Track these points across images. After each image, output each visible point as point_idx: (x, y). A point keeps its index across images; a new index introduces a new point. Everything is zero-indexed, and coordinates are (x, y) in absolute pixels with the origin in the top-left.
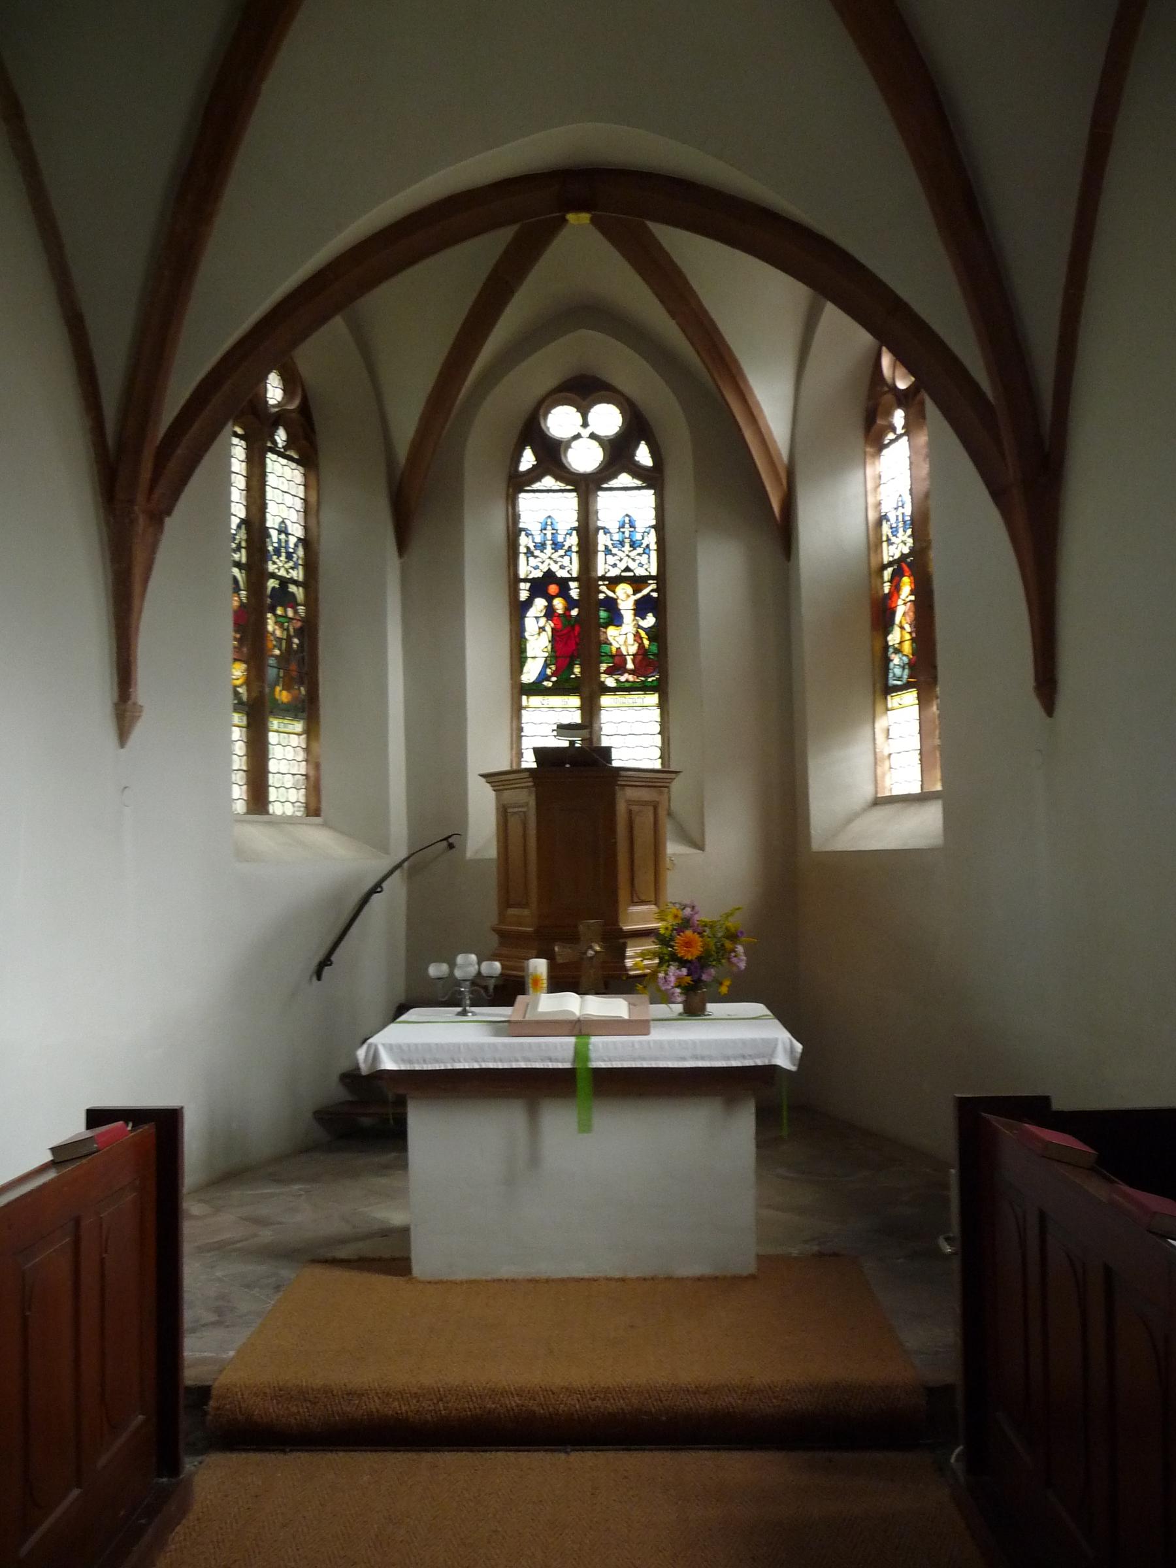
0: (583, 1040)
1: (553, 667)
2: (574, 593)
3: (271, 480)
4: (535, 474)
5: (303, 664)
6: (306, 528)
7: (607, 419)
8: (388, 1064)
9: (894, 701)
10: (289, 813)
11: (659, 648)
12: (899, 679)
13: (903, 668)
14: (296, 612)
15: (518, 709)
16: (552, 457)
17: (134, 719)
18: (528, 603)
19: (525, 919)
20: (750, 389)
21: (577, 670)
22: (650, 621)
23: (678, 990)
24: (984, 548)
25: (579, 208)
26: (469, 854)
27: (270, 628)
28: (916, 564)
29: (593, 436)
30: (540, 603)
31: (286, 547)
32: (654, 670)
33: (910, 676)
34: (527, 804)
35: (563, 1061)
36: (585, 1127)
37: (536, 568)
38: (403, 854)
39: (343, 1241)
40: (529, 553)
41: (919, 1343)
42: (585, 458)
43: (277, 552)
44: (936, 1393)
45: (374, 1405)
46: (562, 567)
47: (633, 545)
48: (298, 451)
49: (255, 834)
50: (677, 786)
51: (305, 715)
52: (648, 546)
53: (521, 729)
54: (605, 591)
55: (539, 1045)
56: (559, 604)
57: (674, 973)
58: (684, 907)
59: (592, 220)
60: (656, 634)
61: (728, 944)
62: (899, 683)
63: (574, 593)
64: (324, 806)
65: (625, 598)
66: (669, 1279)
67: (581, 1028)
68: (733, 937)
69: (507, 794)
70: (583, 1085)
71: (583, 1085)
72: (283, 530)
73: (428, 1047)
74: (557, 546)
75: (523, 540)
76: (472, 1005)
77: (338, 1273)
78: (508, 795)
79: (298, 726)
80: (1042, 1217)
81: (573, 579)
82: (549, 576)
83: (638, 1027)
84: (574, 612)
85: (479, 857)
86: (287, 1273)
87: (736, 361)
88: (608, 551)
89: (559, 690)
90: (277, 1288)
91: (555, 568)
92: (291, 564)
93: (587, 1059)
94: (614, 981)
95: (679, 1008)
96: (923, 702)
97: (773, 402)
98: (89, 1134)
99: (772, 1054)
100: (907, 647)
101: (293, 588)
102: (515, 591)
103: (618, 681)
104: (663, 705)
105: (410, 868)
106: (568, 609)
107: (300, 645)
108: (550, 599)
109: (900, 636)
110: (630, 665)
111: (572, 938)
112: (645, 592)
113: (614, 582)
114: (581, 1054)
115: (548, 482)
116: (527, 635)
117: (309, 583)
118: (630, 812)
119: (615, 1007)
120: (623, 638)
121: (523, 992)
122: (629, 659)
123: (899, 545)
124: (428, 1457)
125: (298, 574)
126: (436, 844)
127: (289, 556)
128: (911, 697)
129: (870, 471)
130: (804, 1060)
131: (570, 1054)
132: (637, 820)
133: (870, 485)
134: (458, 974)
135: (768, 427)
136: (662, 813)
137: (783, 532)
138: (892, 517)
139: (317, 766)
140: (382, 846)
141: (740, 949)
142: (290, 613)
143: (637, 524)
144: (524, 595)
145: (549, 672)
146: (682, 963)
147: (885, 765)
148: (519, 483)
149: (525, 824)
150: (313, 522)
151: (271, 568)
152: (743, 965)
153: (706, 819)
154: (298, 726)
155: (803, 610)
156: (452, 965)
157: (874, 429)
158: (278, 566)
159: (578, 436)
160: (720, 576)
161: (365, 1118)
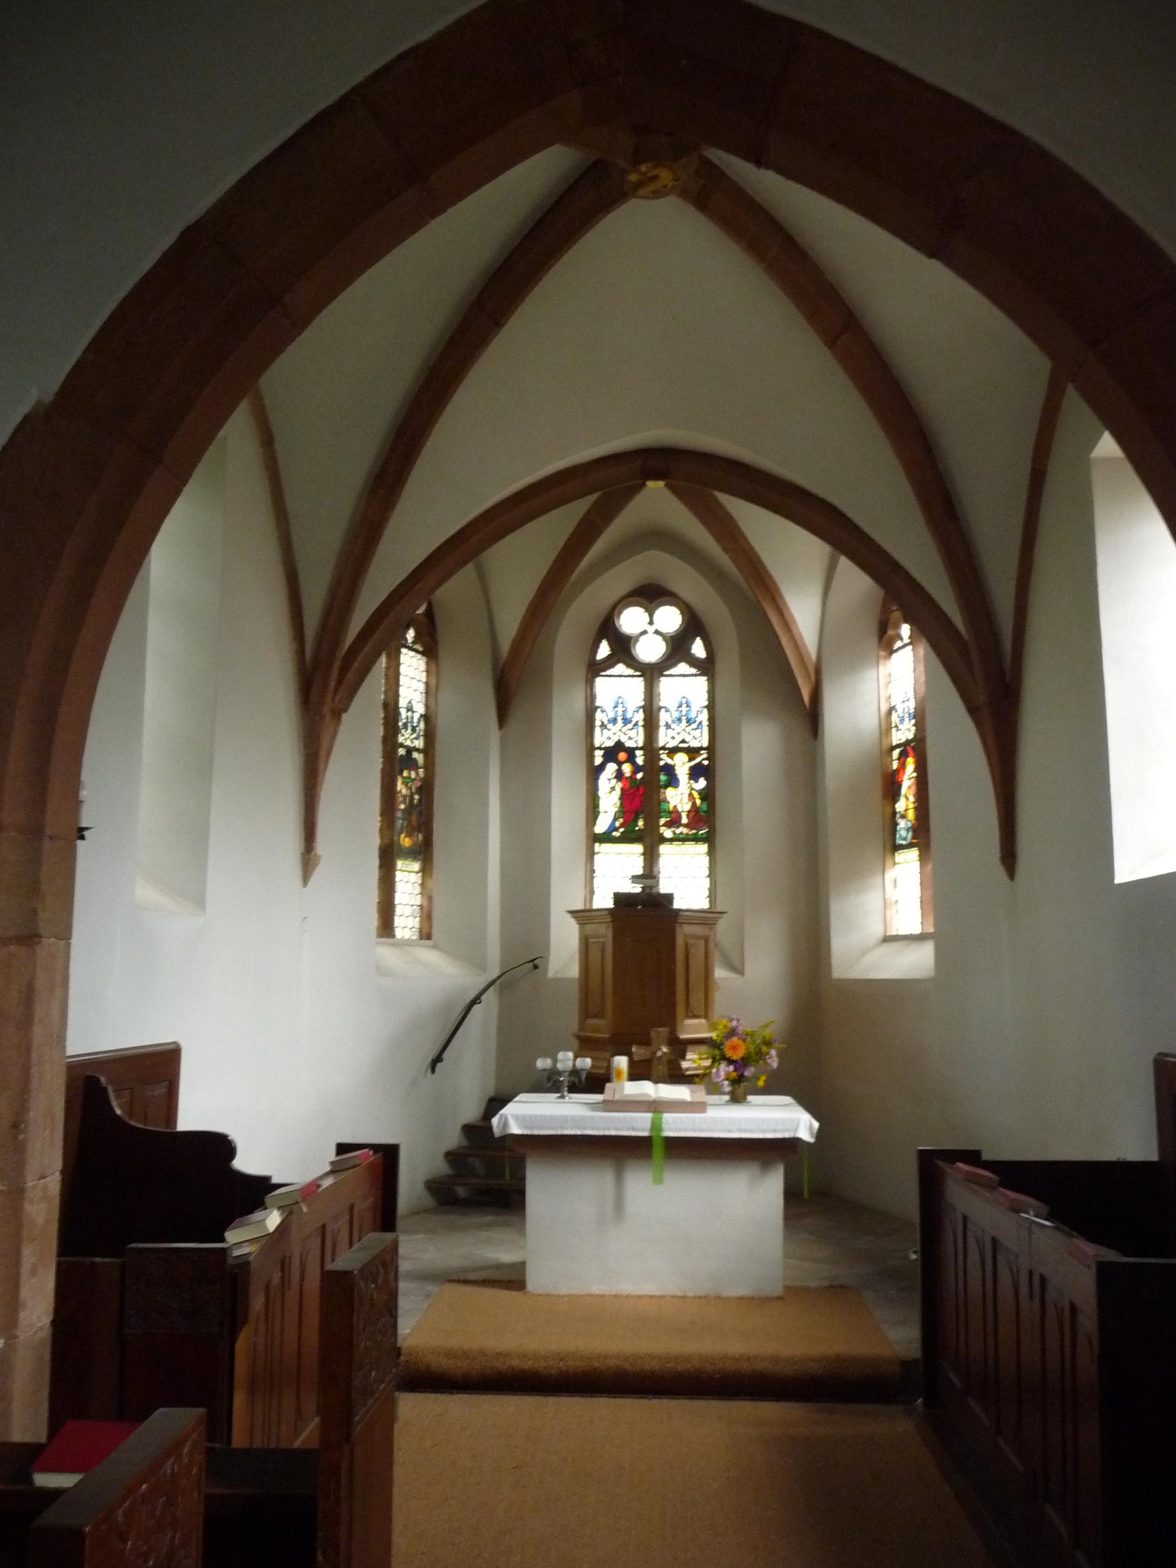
0: (658, 1115)
1: (621, 820)
2: (640, 760)
3: (403, 669)
4: (610, 662)
5: (422, 818)
6: (427, 706)
7: (670, 618)
8: (515, 1129)
9: (900, 856)
10: (407, 937)
11: (708, 805)
12: (905, 839)
13: (908, 830)
14: (417, 774)
15: (591, 854)
16: (623, 648)
17: (315, 865)
18: (602, 767)
19: (602, 1027)
20: (785, 604)
21: (641, 823)
22: (702, 783)
23: (726, 1083)
24: (962, 747)
25: (656, 477)
26: (550, 974)
27: (399, 788)
28: (917, 747)
29: (657, 632)
30: (611, 767)
31: (412, 722)
32: (705, 824)
33: (913, 838)
34: (605, 937)
35: (643, 1130)
36: (659, 1181)
37: (609, 738)
38: (497, 973)
39: (474, 1270)
40: (603, 726)
41: (898, 1336)
42: (650, 650)
43: (405, 726)
44: (906, 1365)
45: (515, 1362)
46: (630, 738)
47: (689, 721)
48: (423, 645)
49: (385, 953)
50: (722, 925)
51: (421, 857)
52: (700, 723)
53: (593, 871)
54: (665, 759)
55: (625, 1118)
56: (627, 769)
57: (724, 1069)
58: (731, 1020)
59: (667, 485)
61: (764, 1049)
62: (904, 843)
63: (640, 760)
64: (435, 932)
65: (682, 765)
66: (719, 1297)
67: (656, 1107)
68: (768, 1043)
69: (588, 927)
70: (658, 1149)
71: (658, 1149)
72: (410, 709)
73: (544, 1118)
74: (626, 721)
75: (599, 717)
76: (570, 1091)
77: (468, 1289)
78: (589, 928)
79: (416, 866)
80: (965, 1218)
81: (637, 748)
82: (619, 746)
83: (700, 1107)
84: (639, 776)
85: (559, 976)
86: (432, 1288)
87: (775, 584)
88: (668, 726)
89: (625, 839)
90: (428, 1296)
91: (624, 739)
92: (414, 735)
93: (661, 1130)
94: (677, 1077)
95: (727, 1098)
96: (923, 858)
97: (804, 612)
98: (339, 1158)
99: (796, 1130)
100: (911, 814)
101: (415, 755)
102: (591, 757)
103: (674, 833)
104: (711, 853)
105: (501, 984)
106: (634, 773)
107: (420, 800)
108: (620, 764)
109: (905, 804)
110: (685, 820)
111: (646, 1042)
112: (698, 760)
113: (673, 751)
114: (656, 1126)
115: (620, 668)
116: (600, 793)
117: (428, 750)
118: (687, 945)
119: (681, 1092)
121: (609, 1080)
122: (684, 815)
123: (904, 732)
124: (552, 1400)
125: (419, 743)
126: (522, 968)
127: (414, 729)
128: (914, 853)
129: (882, 669)
130: (820, 1135)
131: (648, 1125)
132: (692, 951)
133: (882, 682)
134: (560, 1066)
135: (800, 634)
136: (711, 945)
137: (812, 717)
138: (900, 708)
139: (430, 899)
140: (481, 966)
141: (773, 1052)
142: (413, 775)
143: (692, 705)
144: (598, 760)
145: (617, 824)
146: (730, 1062)
147: (889, 913)
148: (596, 669)
149: (603, 951)
150: (432, 701)
151: (401, 739)
152: (775, 1065)
153: (746, 944)
154: (416, 866)
155: (828, 780)
156: (555, 1061)
157: (886, 637)
158: (406, 738)
159: (644, 632)
160: (760, 745)
161: (487, 1177)
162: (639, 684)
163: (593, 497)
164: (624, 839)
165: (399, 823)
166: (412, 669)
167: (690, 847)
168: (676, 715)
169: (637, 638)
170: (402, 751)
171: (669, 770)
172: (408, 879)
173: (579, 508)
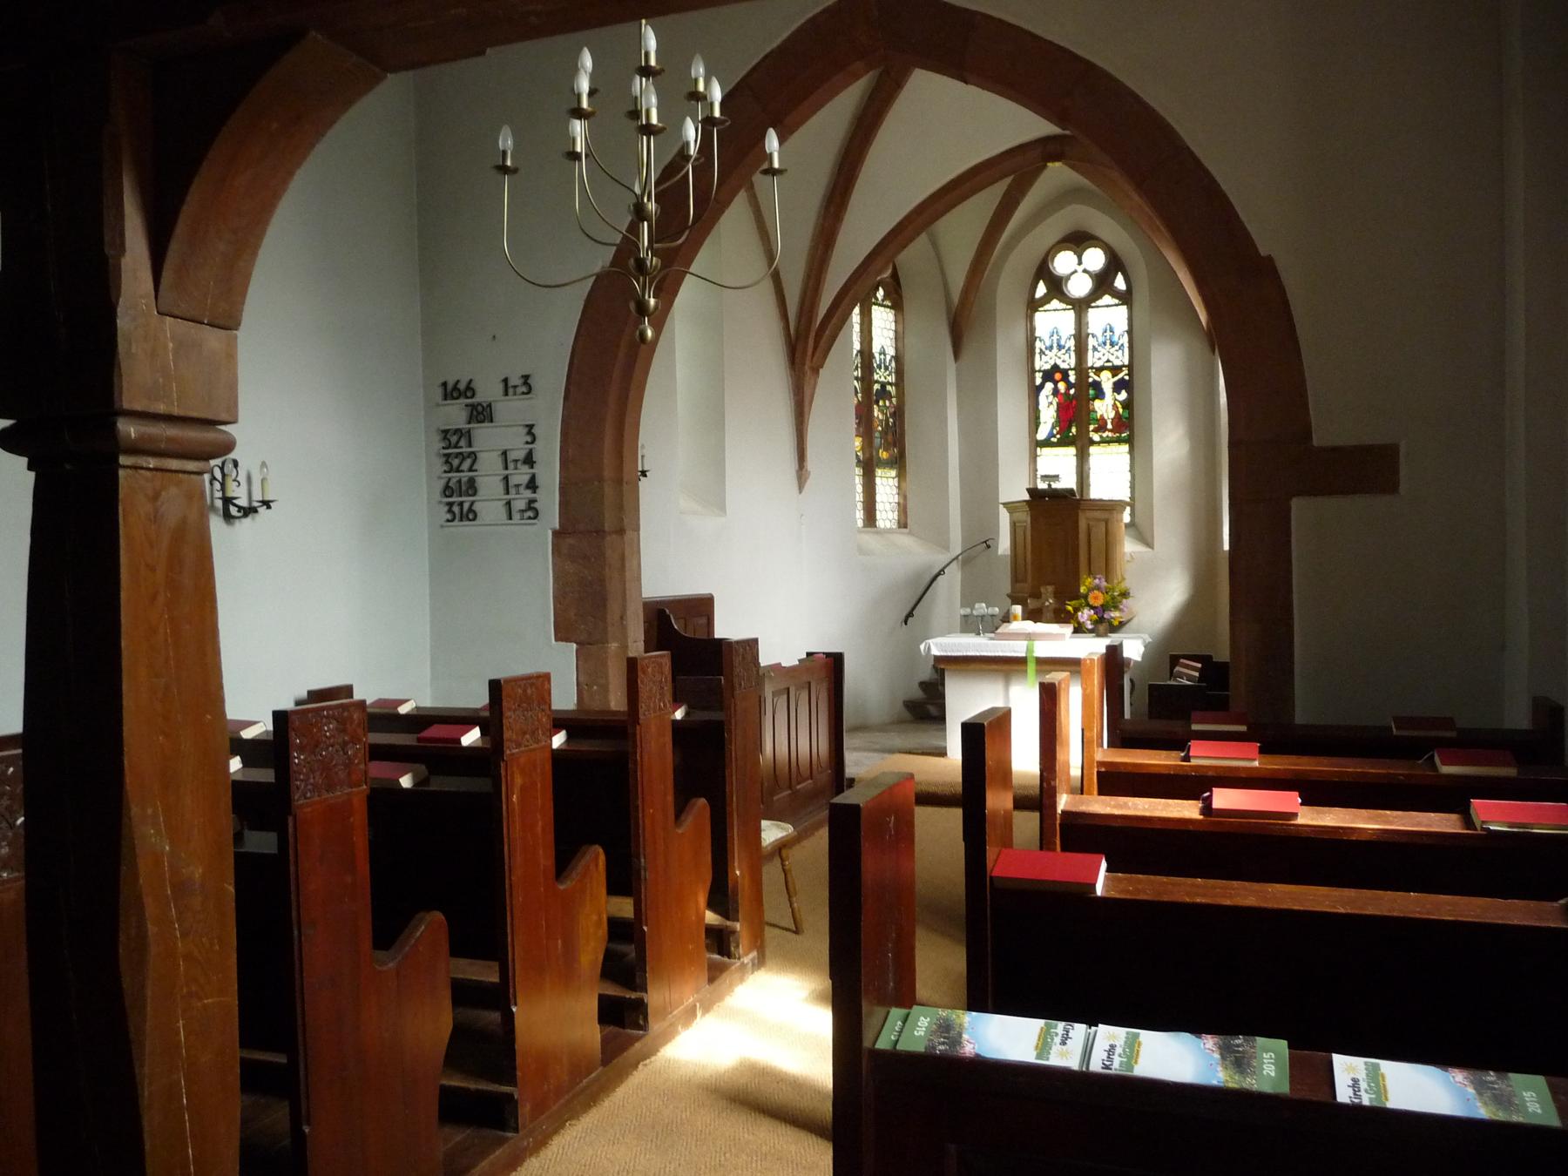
2: (1072, 378)
4: (1046, 300)
5: (896, 436)
6: (896, 349)
7: (1095, 258)
16: (1057, 287)
18: (1042, 386)
19: (1026, 587)
22: (1123, 395)
29: (1085, 271)
30: (1049, 386)
32: (1127, 428)
40: (1042, 352)
42: (1080, 286)
47: (1112, 344)
49: (869, 539)
54: (1093, 377)
60: (1127, 405)
63: (1072, 378)
65: (1107, 381)
67: (1029, 637)
70: (1031, 667)
72: (883, 353)
74: (1060, 347)
75: (1038, 345)
79: (893, 473)
82: (1055, 368)
84: (1072, 391)
88: (1095, 349)
89: (1063, 443)
91: (1059, 362)
101: (889, 388)
102: (1033, 379)
104: (1131, 452)
106: (1068, 389)
108: (1056, 383)
110: (1110, 426)
113: (1099, 370)
114: (1029, 650)
117: (899, 383)
120: (1105, 408)
125: (892, 379)
126: (979, 546)
132: (1094, 530)
139: (905, 497)
144: (1038, 381)
146: (1092, 607)
148: (1034, 305)
151: (876, 377)
154: (893, 473)
158: (880, 376)
162: (1070, 316)
163: (1008, 180)
164: (1061, 444)
165: (877, 441)
166: (883, 319)
167: (1115, 447)
168: (1101, 339)
169: (1068, 278)
170: (876, 387)
171: (1097, 386)
172: (886, 483)
173: (990, 197)
